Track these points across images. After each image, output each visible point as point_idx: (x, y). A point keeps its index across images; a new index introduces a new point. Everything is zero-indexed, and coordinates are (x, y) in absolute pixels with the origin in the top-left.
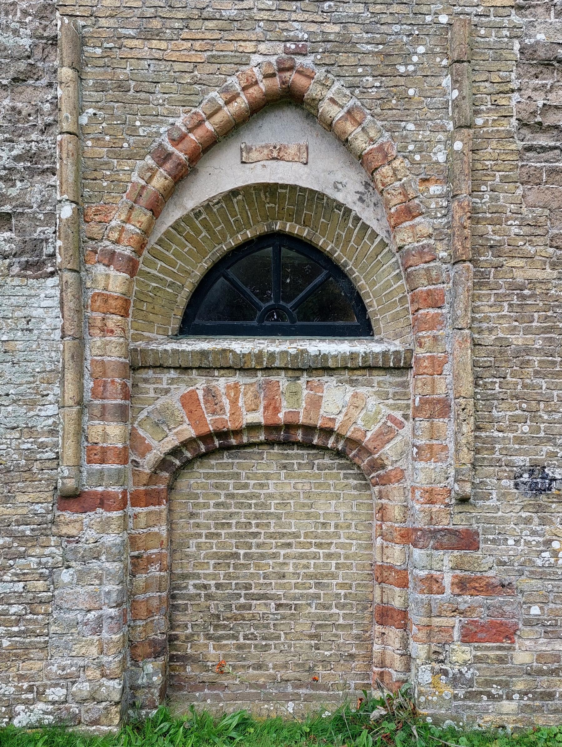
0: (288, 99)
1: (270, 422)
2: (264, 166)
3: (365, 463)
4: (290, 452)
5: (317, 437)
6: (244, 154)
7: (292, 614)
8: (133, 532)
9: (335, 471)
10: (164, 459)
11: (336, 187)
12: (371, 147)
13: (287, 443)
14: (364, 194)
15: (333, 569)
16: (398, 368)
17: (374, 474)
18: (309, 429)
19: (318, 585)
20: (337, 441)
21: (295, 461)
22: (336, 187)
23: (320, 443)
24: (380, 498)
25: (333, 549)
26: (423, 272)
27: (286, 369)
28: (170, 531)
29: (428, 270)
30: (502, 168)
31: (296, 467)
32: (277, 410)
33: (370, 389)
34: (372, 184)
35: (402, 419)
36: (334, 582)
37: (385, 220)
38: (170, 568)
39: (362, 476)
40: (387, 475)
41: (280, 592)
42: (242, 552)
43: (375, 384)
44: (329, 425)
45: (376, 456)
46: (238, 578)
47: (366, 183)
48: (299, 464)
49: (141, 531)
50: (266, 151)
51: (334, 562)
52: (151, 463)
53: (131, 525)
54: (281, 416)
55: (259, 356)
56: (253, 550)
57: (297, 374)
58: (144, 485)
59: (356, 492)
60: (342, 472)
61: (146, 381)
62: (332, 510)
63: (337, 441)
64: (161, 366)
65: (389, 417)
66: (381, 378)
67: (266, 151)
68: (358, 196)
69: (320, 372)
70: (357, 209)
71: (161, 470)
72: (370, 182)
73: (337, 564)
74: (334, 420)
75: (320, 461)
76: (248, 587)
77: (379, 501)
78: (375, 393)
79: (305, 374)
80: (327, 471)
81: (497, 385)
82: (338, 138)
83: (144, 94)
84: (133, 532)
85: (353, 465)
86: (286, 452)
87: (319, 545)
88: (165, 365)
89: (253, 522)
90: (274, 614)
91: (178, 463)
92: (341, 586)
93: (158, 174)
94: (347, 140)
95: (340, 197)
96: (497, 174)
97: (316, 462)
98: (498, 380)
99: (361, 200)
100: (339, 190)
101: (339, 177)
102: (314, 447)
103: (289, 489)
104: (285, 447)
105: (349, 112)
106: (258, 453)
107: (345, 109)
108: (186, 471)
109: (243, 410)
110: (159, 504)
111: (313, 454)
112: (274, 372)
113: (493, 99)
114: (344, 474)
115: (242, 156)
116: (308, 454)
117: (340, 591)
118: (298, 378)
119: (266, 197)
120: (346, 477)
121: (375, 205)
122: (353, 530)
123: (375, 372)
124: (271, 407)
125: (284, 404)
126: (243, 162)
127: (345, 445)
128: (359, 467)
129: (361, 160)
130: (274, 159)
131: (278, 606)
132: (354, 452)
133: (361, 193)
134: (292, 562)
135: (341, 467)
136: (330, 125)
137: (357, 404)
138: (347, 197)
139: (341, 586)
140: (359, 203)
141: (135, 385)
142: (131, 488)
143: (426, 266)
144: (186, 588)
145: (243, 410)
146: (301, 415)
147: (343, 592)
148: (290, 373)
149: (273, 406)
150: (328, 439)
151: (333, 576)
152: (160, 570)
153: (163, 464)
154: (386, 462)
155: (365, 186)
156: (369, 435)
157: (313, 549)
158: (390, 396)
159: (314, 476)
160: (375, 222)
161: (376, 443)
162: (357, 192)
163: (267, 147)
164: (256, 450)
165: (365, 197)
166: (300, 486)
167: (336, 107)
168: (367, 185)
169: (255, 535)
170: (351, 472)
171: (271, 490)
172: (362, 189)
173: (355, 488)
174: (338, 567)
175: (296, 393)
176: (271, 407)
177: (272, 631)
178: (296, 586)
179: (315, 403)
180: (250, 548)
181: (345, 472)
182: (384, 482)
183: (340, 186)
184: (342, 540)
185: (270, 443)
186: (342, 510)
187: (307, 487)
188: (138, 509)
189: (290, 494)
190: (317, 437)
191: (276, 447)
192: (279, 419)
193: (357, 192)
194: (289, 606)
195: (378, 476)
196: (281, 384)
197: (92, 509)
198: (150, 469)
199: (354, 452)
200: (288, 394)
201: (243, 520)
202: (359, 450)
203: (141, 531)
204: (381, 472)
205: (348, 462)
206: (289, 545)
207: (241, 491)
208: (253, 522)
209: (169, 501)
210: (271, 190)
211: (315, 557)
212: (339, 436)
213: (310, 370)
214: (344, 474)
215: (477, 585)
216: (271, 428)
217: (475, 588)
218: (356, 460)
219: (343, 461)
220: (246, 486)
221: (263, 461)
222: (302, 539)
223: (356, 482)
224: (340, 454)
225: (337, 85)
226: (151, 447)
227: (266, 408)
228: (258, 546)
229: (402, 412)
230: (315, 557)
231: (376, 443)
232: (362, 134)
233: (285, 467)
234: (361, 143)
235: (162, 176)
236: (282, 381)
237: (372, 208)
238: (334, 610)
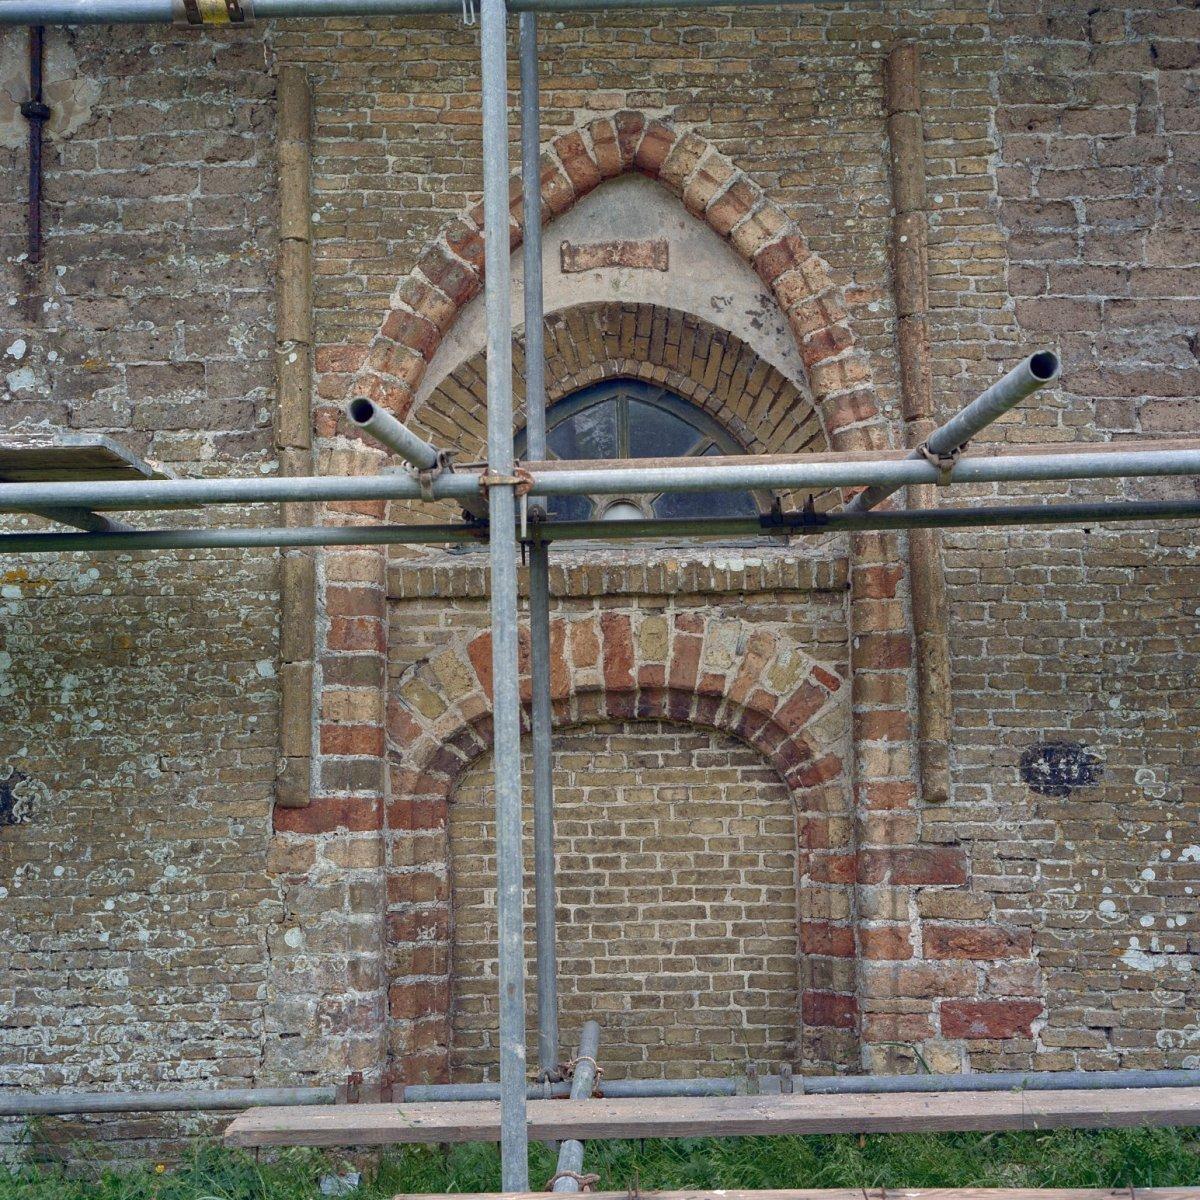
0: (640, 169)
1: (615, 685)
2: (598, 276)
3: (777, 750)
4: (650, 736)
5: (694, 708)
6: (567, 259)
7: (662, 1015)
8: (393, 871)
9: (728, 767)
10: (441, 749)
11: (715, 306)
12: (767, 244)
13: (647, 720)
14: (760, 315)
15: (729, 935)
16: (826, 591)
17: (792, 770)
18: (682, 694)
19: (704, 964)
20: (729, 715)
21: (659, 753)
22: (715, 306)
23: (701, 719)
24: (805, 810)
25: (728, 901)
26: (859, 434)
27: (641, 595)
28: (451, 873)
29: (865, 430)
30: (977, 270)
31: (661, 762)
32: (627, 663)
33: (780, 625)
34: (773, 299)
35: (835, 674)
36: (732, 957)
37: (795, 354)
38: (451, 935)
39: (774, 775)
40: (815, 767)
41: (640, 977)
42: (572, 908)
43: (789, 618)
44: (716, 686)
45: (794, 736)
46: (567, 952)
47: (763, 297)
48: (666, 757)
49: (404, 869)
50: (601, 254)
51: (729, 924)
52: (421, 755)
53: (389, 859)
54: (633, 672)
55: (594, 572)
56: (592, 904)
57: (659, 603)
58: (410, 792)
59: (764, 803)
60: (740, 769)
61: (415, 621)
62: (725, 834)
63: (729, 715)
64: (436, 598)
65: (816, 671)
66: (798, 607)
67: (601, 254)
68: (751, 318)
69: (696, 600)
70: (749, 336)
71: (436, 769)
72: (768, 295)
73: (735, 926)
74: (723, 677)
75: (703, 751)
76: (583, 967)
77: (803, 814)
78: (790, 632)
79: (672, 602)
80: (714, 768)
81: (987, 612)
82: (717, 232)
83: (798, 421)
84: (393, 871)
85: (760, 755)
86: (643, 737)
87: (703, 894)
88: (443, 594)
89: (591, 857)
90: (630, 1014)
91: (463, 756)
92: (742, 964)
93: (431, 296)
94: (730, 234)
95: (721, 320)
96: (972, 278)
97: (696, 752)
98: (986, 604)
99: (756, 324)
100: (719, 310)
101: (719, 288)
102: (688, 726)
103: (647, 800)
104: (641, 727)
105: (730, 191)
106: (597, 740)
107: (726, 187)
108: (475, 772)
109: (571, 665)
110: (434, 825)
111: (690, 739)
112: (621, 601)
113: (960, 165)
114: (743, 772)
115: (563, 262)
116: (682, 740)
117: (741, 972)
118: (661, 610)
119: (602, 323)
120: (747, 777)
121: (779, 331)
122: (761, 866)
123: (788, 599)
124: (617, 660)
125: (638, 653)
126: (564, 271)
127: (744, 720)
128: (767, 760)
129: (757, 265)
130: (613, 264)
131: (638, 1001)
132: (758, 733)
133: (755, 313)
134: (657, 923)
135: (738, 760)
136: (703, 212)
137: (754, 648)
138: (734, 320)
139: (742, 964)
140: (753, 330)
141: (394, 628)
142: (390, 798)
143: (861, 424)
144: (480, 971)
145: (571, 665)
146: (667, 671)
147: (746, 974)
148: (647, 603)
149: (618, 656)
150: (713, 712)
151: (731, 947)
152: (437, 938)
153: (438, 759)
154: (811, 745)
155: (762, 301)
156: (782, 702)
157: (693, 902)
158: (815, 636)
159: (693, 776)
160: (779, 357)
161: (796, 714)
162: (750, 313)
163: (602, 246)
164: (592, 732)
165: (761, 320)
166: (669, 794)
167: (710, 185)
168: (764, 300)
169: (598, 880)
170: (756, 768)
171: (621, 802)
172: (757, 307)
173: (763, 795)
174: (739, 930)
175: (658, 636)
176: (617, 660)
177: (626, 1044)
178: (670, 965)
179: (689, 651)
180: (587, 901)
181: (745, 768)
182: (809, 781)
183: (721, 304)
184: (744, 884)
185: (617, 721)
186: (740, 835)
187: (680, 796)
188: (400, 833)
189: (652, 808)
190: (694, 708)
191: (596, 604)
192: (631, 679)
193: (750, 313)
194: (653, 1001)
195: (799, 772)
196: (632, 620)
197: (330, 827)
198: (419, 766)
199: (758, 733)
200: (644, 638)
201: (574, 854)
202: (767, 730)
203: (404, 869)
204: (805, 765)
205: (750, 751)
206: (653, 895)
207: (568, 806)
208: (591, 857)
209: (449, 822)
210: (616, 313)
211: (700, 913)
212: (733, 705)
213: (683, 595)
214: (743, 772)
215: (966, 942)
216: (618, 694)
217: (962, 947)
218: (763, 745)
219: (741, 751)
220: (578, 796)
221: (606, 754)
222: (674, 885)
223: (764, 785)
224: (737, 738)
225: (711, 150)
226: (420, 729)
227: (608, 661)
228: (601, 897)
229: (835, 662)
230: (700, 913)
231: (796, 714)
232: (752, 223)
233: (642, 762)
234: (752, 239)
235: (438, 297)
236: (634, 614)
237: (774, 337)
238: (733, 1006)
